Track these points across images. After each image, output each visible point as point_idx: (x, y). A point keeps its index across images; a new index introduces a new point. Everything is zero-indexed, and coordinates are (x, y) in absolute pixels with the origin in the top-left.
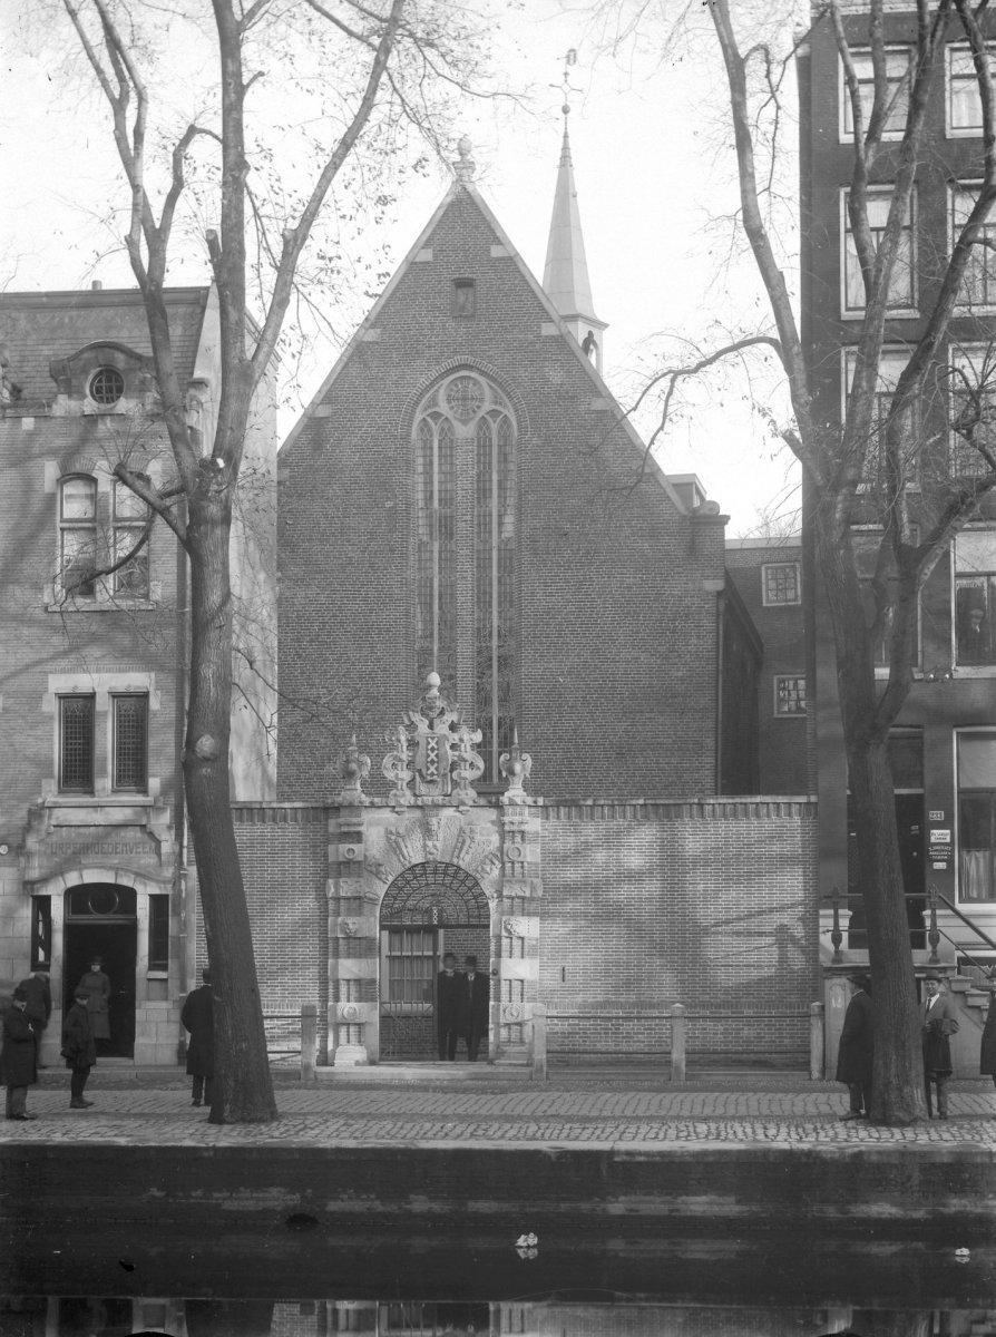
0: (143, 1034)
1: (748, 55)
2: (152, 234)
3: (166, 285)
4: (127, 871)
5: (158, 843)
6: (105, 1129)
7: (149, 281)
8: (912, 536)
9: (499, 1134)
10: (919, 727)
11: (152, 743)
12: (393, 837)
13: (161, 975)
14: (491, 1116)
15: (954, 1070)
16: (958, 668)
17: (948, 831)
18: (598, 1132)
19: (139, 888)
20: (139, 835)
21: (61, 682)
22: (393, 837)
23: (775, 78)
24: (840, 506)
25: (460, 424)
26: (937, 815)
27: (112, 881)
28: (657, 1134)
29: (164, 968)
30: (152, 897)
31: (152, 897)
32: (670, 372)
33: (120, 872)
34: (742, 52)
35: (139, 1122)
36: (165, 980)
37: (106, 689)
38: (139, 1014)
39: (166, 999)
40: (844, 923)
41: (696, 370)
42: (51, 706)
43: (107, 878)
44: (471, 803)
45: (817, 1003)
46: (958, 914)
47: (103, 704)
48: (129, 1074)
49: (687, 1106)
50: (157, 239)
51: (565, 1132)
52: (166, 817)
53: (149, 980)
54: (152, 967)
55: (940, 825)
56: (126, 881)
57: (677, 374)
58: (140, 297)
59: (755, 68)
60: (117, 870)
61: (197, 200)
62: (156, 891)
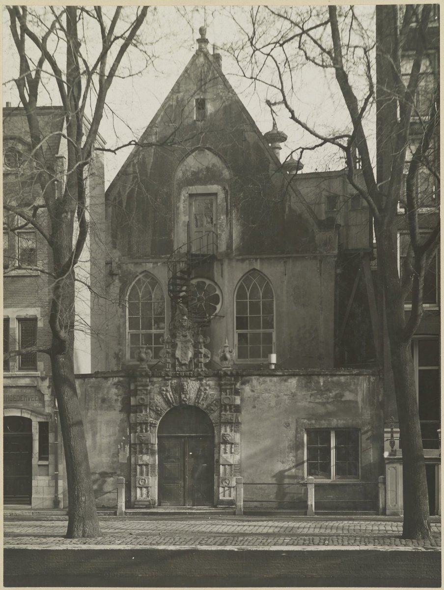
5: (43, 395)
8: (355, 150)
9: (214, 542)
12: (164, 392)
14: (252, 533)
15: (119, 507)
18: (264, 541)
19: (33, 418)
20: (33, 391)
22: (164, 392)
24: (376, 208)
25: (219, 197)
27: (19, 415)
28: (294, 542)
29: (47, 459)
30: (40, 423)
31: (40, 423)
32: (300, 148)
36: (47, 466)
37: (15, 316)
40: (397, 436)
41: (313, 148)
44: (204, 375)
45: (382, 476)
48: (27, 513)
50: (34, 85)
52: (46, 383)
53: (39, 465)
54: (40, 459)
57: (303, 149)
62: (43, 420)
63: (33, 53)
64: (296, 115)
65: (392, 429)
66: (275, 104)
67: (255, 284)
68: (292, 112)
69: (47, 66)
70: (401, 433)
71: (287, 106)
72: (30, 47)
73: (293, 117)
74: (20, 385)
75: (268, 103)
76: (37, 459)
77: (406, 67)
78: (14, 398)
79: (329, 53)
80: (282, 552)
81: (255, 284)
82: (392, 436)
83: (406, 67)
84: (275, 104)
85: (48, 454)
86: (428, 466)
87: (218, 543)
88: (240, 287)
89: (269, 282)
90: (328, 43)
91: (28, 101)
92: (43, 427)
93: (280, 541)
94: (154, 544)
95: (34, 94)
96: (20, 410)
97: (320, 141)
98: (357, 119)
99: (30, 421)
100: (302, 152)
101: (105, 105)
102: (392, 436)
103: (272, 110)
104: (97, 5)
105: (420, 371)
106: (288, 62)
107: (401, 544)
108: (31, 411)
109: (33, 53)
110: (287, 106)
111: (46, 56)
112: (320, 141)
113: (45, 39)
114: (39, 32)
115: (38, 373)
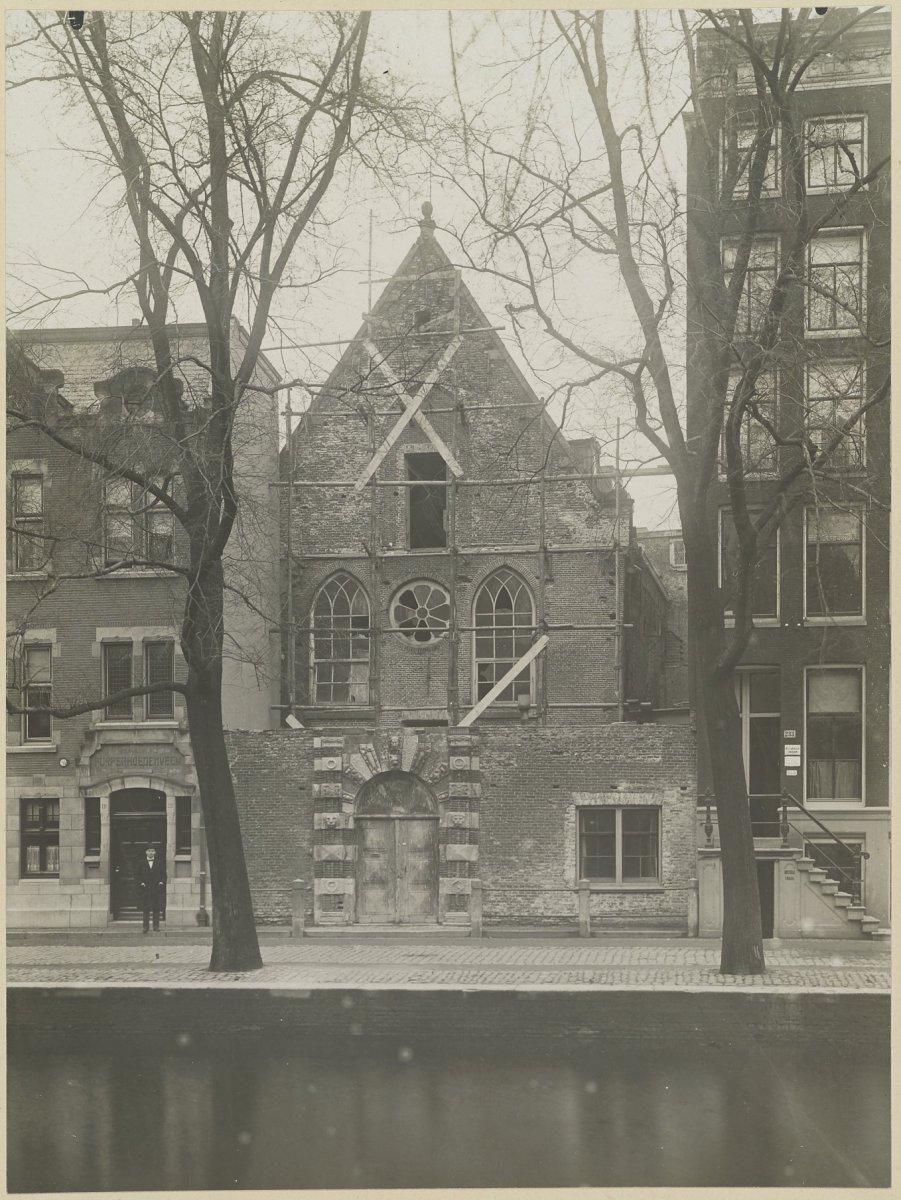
0: (174, 903)
1: (623, 134)
2: (152, 279)
3: (205, 322)
4: (159, 778)
6: (130, 976)
7: (156, 316)
10: (777, 665)
11: (426, 718)
13: (186, 858)
16: (808, 618)
17: (799, 746)
18: (508, 977)
19: (167, 791)
21: (104, 633)
23: (648, 154)
26: (790, 734)
27: (146, 786)
29: (188, 852)
30: (178, 799)
32: (567, 384)
33: (153, 780)
34: (619, 130)
35: (156, 970)
38: (169, 888)
39: (190, 876)
42: (96, 650)
43: (144, 784)
46: (804, 811)
47: (137, 651)
49: (584, 958)
51: (456, 977)
52: (187, 739)
54: (178, 852)
55: (791, 741)
56: (157, 787)
57: (572, 386)
58: (206, 330)
59: (629, 142)
60: (151, 778)
61: (317, 263)
63: (162, 243)
64: (555, 326)
65: (708, 808)
66: (521, 309)
67: (504, 588)
68: (548, 321)
69: (182, 261)
70: (718, 812)
71: (541, 313)
72: (155, 228)
73: (551, 330)
74: (147, 741)
75: (510, 308)
76: (174, 853)
77: (730, 257)
78: (140, 761)
79: (610, 233)
80: (717, 548)
81: (504, 588)
82: (708, 818)
83: (730, 257)
84: (521, 309)
85: (190, 845)
86: (761, 864)
87: (439, 980)
88: (480, 598)
89: (526, 587)
90: (608, 217)
91: (152, 310)
92: (183, 805)
93: (533, 977)
94: (340, 981)
95: (162, 302)
96: (148, 780)
97: (599, 369)
98: (650, 326)
99: (163, 795)
100: (569, 391)
101: (269, 320)
102: (708, 818)
103: (514, 319)
104: (68, 7)
105: (751, 719)
106: (622, 364)
107: (718, 982)
108: (165, 780)
109: (162, 243)
110: (541, 313)
111: (180, 242)
112: (599, 369)
113: (180, 218)
114: (171, 210)
115: (174, 723)
